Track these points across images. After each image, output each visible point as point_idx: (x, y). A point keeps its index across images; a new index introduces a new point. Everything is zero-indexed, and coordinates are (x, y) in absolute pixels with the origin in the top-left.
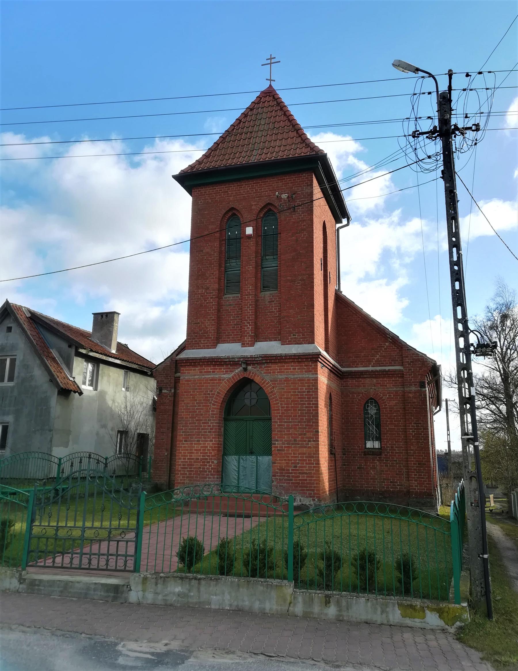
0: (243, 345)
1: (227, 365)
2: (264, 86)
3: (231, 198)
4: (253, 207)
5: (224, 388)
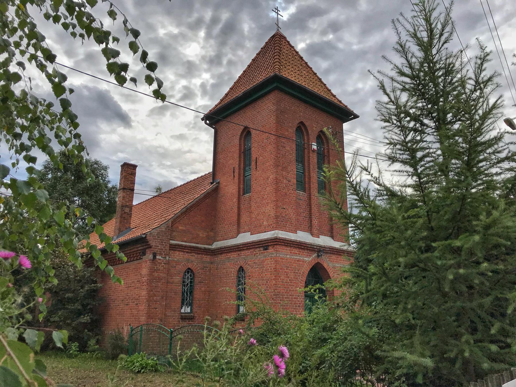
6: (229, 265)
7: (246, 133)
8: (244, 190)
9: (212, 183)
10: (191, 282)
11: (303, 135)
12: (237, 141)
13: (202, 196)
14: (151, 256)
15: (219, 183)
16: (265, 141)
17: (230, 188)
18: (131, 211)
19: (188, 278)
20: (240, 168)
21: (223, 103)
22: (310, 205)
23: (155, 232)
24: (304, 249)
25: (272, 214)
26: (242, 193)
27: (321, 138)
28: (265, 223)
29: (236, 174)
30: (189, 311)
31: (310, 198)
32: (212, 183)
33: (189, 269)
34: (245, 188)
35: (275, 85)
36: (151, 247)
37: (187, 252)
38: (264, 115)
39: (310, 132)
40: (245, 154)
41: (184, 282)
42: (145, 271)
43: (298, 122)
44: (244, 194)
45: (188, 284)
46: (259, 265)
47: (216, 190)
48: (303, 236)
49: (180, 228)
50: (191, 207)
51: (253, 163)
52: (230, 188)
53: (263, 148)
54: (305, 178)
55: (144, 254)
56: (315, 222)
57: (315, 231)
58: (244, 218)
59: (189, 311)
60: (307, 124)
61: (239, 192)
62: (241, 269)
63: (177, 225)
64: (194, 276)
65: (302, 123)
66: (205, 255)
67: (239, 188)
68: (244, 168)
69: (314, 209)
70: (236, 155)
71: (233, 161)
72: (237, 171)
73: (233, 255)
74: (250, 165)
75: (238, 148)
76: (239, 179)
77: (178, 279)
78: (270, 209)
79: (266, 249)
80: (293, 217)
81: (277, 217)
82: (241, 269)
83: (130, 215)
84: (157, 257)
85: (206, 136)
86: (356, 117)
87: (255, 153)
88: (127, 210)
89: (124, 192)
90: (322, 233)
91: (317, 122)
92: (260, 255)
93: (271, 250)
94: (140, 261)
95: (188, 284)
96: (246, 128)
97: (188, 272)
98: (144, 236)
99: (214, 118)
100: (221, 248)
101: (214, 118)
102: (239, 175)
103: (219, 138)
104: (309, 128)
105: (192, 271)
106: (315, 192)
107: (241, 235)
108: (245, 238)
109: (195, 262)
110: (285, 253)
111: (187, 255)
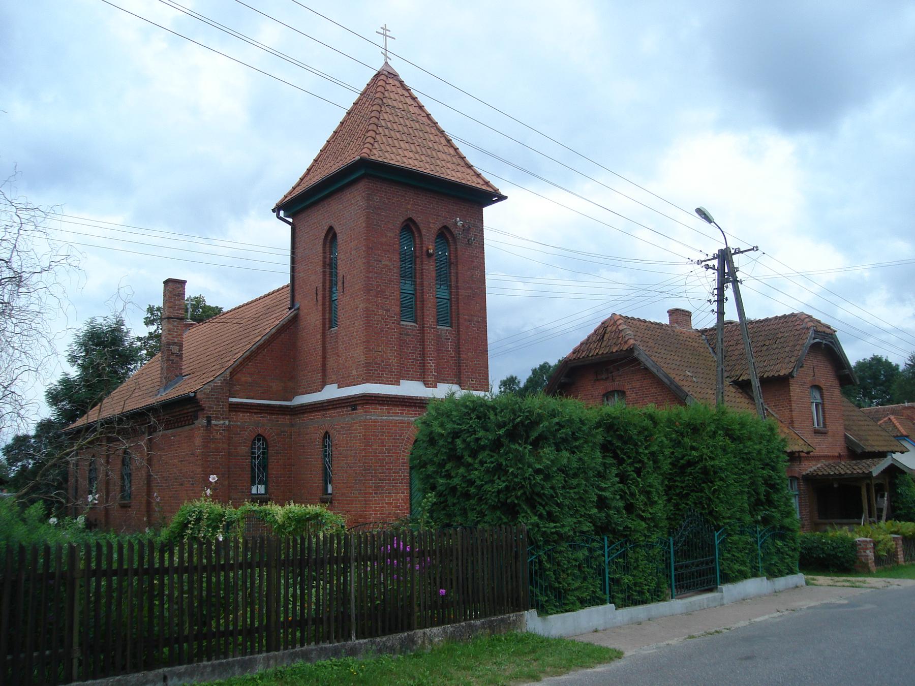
0: (427, 385)
1: (415, 407)
2: (379, 66)
3: (409, 207)
4: (431, 225)
5: (413, 433)
6: (316, 425)
7: (331, 236)
8: (330, 321)
9: (290, 309)
10: (263, 453)
11: (414, 237)
12: (319, 248)
13: (274, 331)
14: (204, 421)
15: (298, 309)
16: (354, 252)
17: (312, 318)
18: (181, 350)
19: (259, 447)
20: (324, 289)
21: (296, 193)
22: (422, 341)
23: (208, 389)
24: (411, 406)
25: (363, 359)
26: (327, 326)
27: (444, 234)
28: (354, 373)
29: (320, 298)
30: (263, 492)
31: (422, 331)
32: (290, 309)
33: (259, 435)
34: (330, 320)
35: (363, 172)
36: (203, 409)
37: (255, 413)
38: (349, 212)
39: (424, 232)
40: (330, 266)
41: (253, 453)
42: (198, 441)
43: (402, 219)
44: (331, 327)
45: (259, 456)
46: (348, 431)
47: (294, 320)
48: (411, 388)
49: (243, 379)
50: (258, 348)
51: (340, 284)
52: (312, 318)
53: (350, 259)
54: (416, 301)
55: (196, 418)
56: (431, 365)
57: (430, 379)
58: (331, 363)
59: (263, 492)
60: (418, 220)
61: (324, 324)
62: (327, 435)
63: (239, 375)
64: (267, 446)
65: (410, 219)
66: (282, 414)
67: (324, 319)
68: (331, 288)
69: (431, 347)
70: (319, 269)
71: (314, 277)
72: (320, 292)
73: (317, 416)
74: (336, 285)
75: (321, 258)
76: (324, 304)
77: (244, 450)
78: (358, 353)
79: (353, 410)
80: (394, 361)
81: (368, 365)
82: (327, 435)
83: (180, 356)
84: (213, 422)
85: (281, 232)
86: (502, 198)
87: (342, 270)
88: (175, 349)
89: (169, 323)
90: (441, 378)
91: (431, 216)
92: (344, 418)
93: (360, 410)
94: (193, 426)
95: (259, 456)
96: (331, 228)
97: (259, 440)
98: (192, 395)
99: (294, 207)
100: (302, 406)
101: (294, 207)
102: (324, 298)
103: (297, 240)
104: (421, 226)
105: (264, 439)
106: (430, 320)
107: (328, 387)
108: (331, 392)
109: (266, 425)
110: (379, 415)
111: (255, 417)
